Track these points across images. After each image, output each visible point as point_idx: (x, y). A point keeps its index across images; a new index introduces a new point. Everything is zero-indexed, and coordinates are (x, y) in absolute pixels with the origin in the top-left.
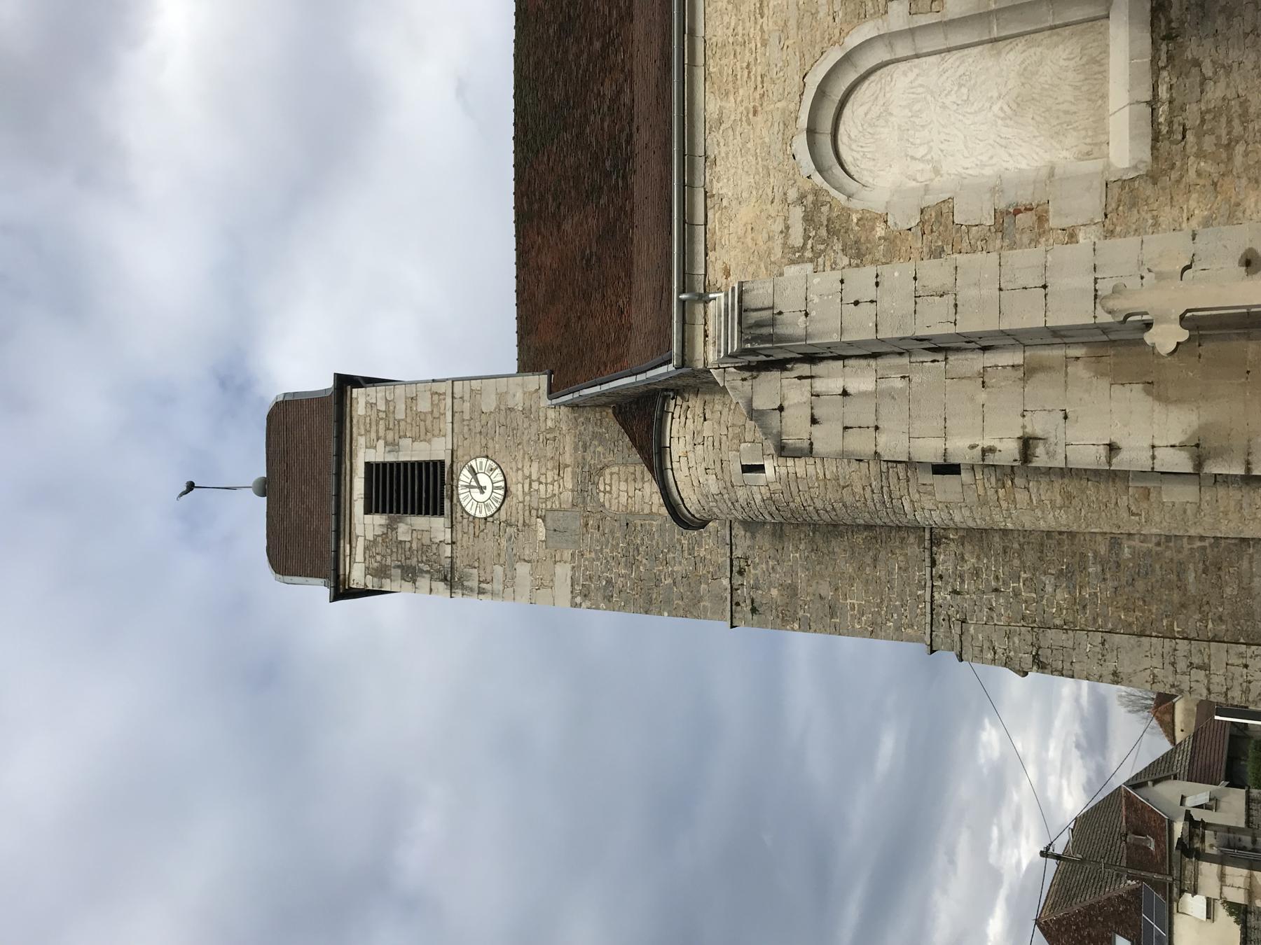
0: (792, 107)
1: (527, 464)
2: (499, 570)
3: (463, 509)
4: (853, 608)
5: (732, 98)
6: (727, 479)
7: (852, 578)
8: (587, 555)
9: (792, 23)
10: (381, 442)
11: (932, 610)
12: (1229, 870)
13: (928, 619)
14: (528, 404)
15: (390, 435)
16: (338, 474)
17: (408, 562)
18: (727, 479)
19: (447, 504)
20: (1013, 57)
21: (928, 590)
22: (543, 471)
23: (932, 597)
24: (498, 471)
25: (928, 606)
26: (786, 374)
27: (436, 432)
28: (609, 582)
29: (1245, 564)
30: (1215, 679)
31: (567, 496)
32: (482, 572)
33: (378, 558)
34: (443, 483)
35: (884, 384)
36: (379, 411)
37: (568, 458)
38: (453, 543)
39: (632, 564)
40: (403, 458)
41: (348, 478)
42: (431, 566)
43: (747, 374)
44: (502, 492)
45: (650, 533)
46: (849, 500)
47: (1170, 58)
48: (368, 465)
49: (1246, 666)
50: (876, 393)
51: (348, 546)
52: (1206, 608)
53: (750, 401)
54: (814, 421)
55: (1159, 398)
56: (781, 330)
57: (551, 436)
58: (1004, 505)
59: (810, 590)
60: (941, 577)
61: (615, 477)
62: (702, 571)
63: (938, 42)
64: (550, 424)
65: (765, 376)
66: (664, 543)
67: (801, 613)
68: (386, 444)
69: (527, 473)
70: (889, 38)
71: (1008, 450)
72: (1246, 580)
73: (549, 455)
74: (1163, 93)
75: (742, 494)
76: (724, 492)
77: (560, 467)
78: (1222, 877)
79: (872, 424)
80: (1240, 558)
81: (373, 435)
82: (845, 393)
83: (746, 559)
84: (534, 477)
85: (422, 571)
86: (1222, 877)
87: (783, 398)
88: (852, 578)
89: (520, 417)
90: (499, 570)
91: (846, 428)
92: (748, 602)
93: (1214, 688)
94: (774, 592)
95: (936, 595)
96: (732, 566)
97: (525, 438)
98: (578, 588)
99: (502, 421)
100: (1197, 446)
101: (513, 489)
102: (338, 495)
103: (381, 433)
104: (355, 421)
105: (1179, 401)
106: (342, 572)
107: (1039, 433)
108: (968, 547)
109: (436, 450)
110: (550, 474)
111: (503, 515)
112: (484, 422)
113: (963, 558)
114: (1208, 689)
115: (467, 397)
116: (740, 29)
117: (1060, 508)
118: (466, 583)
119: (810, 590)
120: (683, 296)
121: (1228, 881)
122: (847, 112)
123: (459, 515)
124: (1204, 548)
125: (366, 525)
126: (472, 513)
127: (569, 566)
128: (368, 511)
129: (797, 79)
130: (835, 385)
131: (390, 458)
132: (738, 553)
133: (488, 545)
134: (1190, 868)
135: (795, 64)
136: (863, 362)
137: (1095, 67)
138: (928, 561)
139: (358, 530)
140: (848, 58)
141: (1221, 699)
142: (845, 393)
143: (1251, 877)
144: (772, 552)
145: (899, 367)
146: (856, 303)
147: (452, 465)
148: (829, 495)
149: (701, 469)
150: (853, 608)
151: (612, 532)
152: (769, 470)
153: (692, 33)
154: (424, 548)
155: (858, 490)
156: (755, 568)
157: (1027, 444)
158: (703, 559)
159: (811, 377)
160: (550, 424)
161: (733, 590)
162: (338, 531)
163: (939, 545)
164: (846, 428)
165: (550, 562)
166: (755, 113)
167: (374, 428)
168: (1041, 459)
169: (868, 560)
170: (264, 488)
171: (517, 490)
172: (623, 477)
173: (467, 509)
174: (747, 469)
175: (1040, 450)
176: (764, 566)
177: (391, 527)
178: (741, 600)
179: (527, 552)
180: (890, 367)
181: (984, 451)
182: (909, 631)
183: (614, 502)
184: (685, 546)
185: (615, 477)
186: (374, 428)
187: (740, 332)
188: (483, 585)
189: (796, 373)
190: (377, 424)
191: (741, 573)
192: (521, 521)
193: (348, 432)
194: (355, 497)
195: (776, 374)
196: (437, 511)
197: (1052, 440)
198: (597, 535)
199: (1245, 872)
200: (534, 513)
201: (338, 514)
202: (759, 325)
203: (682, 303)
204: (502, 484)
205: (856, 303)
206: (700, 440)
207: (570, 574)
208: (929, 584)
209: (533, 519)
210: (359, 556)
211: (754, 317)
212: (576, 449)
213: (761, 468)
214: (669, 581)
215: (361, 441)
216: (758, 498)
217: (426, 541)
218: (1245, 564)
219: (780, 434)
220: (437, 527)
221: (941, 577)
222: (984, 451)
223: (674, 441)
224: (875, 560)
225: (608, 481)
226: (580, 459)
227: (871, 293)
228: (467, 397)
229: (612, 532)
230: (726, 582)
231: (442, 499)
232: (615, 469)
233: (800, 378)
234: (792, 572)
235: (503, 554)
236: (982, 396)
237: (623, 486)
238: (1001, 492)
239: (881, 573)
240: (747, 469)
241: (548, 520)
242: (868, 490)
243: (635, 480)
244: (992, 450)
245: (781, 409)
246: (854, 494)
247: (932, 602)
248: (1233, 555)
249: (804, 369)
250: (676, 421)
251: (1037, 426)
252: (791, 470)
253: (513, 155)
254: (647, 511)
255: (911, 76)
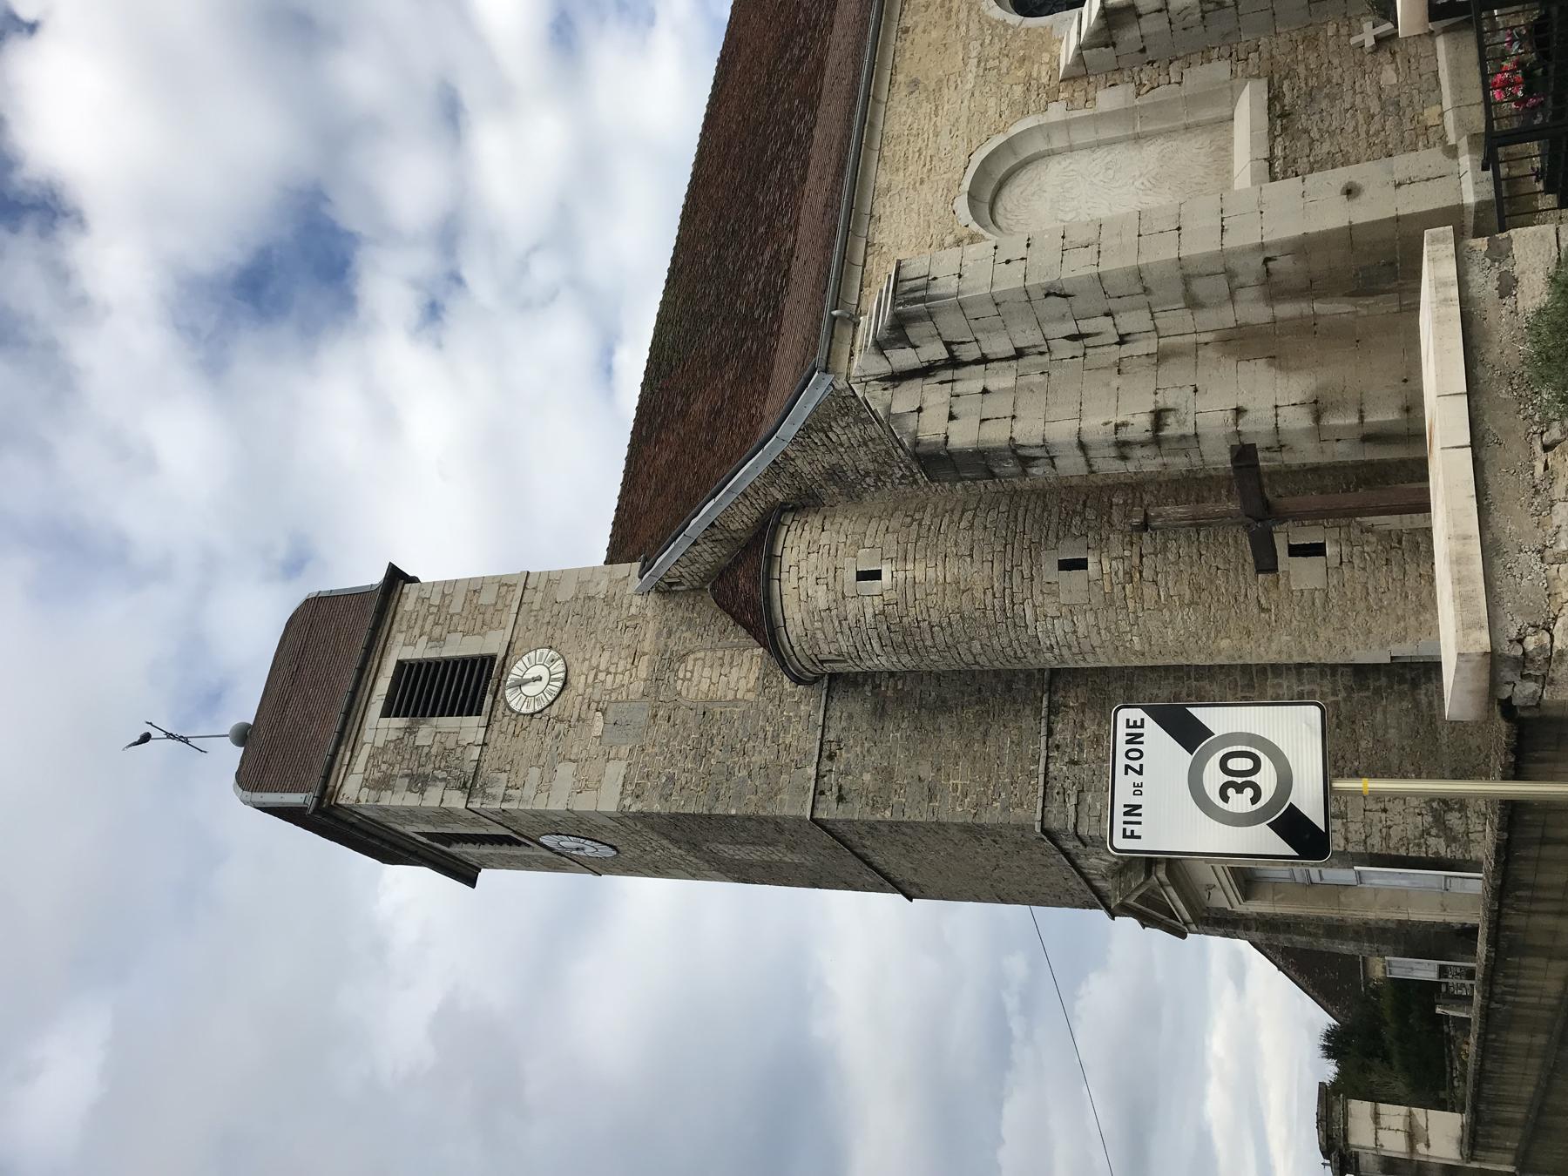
0: (957, 177)
1: (598, 651)
2: (535, 772)
3: (507, 706)
4: (955, 789)
5: (901, 173)
6: (839, 588)
7: (957, 756)
8: (650, 750)
9: (963, 119)
10: (425, 638)
11: (1046, 783)
12: (1383, 1107)
13: (1041, 793)
14: (611, 592)
15: (437, 631)
16: (362, 670)
17: (421, 770)
18: (839, 588)
19: (488, 699)
20: (1152, 151)
21: (1043, 761)
22: (615, 660)
23: (1047, 768)
24: (560, 662)
25: (1041, 778)
26: (929, 380)
27: (496, 623)
28: (671, 778)
29: (1379, 717)
30: (1352, 827)
31: (638, 687)
32: (513, 776)
33: (384, 767)
34: (489, 676)
35: (1023, 381)
36: (430, 605)
37: (647, 646)
38: (484, 744)
39: (702, 756)
40: (449, 651)
41: (386, 628)
42: (449, 773)
43: (888, 384)
44: (560, 684)
45: (730, 722)
46: (967, 608)
47: (1284, 129)
48: (400, 664)
49: (1385, 811)
50: (1015, 389)
51: (348, 754)
52: (1340, 763)
53: (890, 406)
54: (952, 417)
55: (1280, 368)
56: (932, 292)
57: (633, 624)
58: (1131, 604)
59: (908, 772)
60: (1058, 747)
61: (700, 663)
62: (784, 759)
63: (1088, 136)
64: (633, 610)
65: (905, 385)
66: (745, 730)
67: (895, 799)
68: (430, 640)
69: (594, 662)
70: (1046, 130)
71: (1140, 424)
72: (1380, 732)
73: (626, 642)
74: (1278, 152)
75: (852, 607)
76: (833, 606)
77: (635, 656)
78: (1376, 1116)
79: (1009, 413)
80: (1374, 710)
81: (417, 631)
82: (985, 391)
83: (839, 742)
84: (602, 667)
85: (436, 779)
86: (1376, 1116)
87: (923, 400)
88: (957, 756)
89: (600, 604)
90: (535, 772)
91: (983, 421)
92: (835, 789)
93: (1353, 837)
94: (867, 777)
95: (1051, 767)
96: (821, 750)
97: (601, 626)
98: (629, 788)
99: (578, 609)
100: (1316, 402)
101: (573, 680)
102: (354, 693)
103: (427, 629)
104: (398, 618)
105: (1298, 369)
106: (332, 782)
107: (1170, 404)
108: (1089, 714)
109: (492, 644)
110: (622, 663)
111: (555, 710)
112: (555, 611)
113: (1082, 726)
114: (1346, 839)
115: (541, 587)
116: (915, 126)
117: (1189, 606)
118: (488, 791)
119: (908, 772)
120: (835, 313)
121: (1384, 1122)
122: (1005, 192)
123: (499, 714)
124: (1337, 703)
125: (378, 728)
126: (517, 709)
127: (624, 764)
128: (386, 713)
129: (964, 157)
130: (977, 386)
131: (432, 654)
132: (831, 736)
133: (530, 744)
134: (1338, 1108)
135: (963, 146)
136: (1005, 364)
137: (1224, 151)
138: (1044, 731)
139: (367, 735)
140: (1009, 145)
141: (1361, 849)
142: (985, 391)
143: (1411, 1115)
144: (869, 733)
145: (1038, 365)
146: (1008, 262)
147: (505, 658)
148: (948, 604)
149: (812, 579)
150: (955, 790)
151: (684, 722)
152: (886, 576)
153: (872, 125)
154: (446, 753)
155: (979, 595)
156: (848, 752)
157: (1159, 416)
158: (788, 748)
159: (953, 381)
160: (633, 610)
161: (819, 777)
162: (341, 734)
163: (1056, 715)
164: (983, 421)
165: (602, 760)
166: (922, 182)
167: (420, 622)
168: (1172, 429)
169: (977, 736)
170: (243, 736)
171: (578, 682)
172: (708, 663)
173: (512, 705)
174: (863, 576)
175: (1171, 420)
176: (858, 749)
177: (410, 731)
178: (827, 787)
179: (575, 750)
180: (1030, 366)
181: (1117, 426)
182: (1018, 810)
183: (692, 690)
184: (769, 735)
185: (700, 663)
186: (420, 622)
187: (894, 298)
188: (510, 792)
189: (938, 379)
190: (425, 620)
191: (831, 757)
192: (575, 716)
193: (386, 628)
194: (373, 699)
195: (919, 381)
196: (474, 709)
197: (1183, 410)
198: (665, 726)
199: (1403, 1110)
200: (594, 706)
201: (347, 714)
202: (912, 290)
203: (835, 318)
204: (562, 675)
205: (1008, 262)
206: (815, 548)
207: (623, 772)
208: (1044, 754)
209: (591, 713)
210: (359, 766)
211: (908, 285)
212: (659, 635)
213: (876, 575)
214: (744, 773)
215: (400, 638)
216: (869, 611)
217: (450, 744)
218: (1379, 717)
219: (916, 432)
220: (469, 728)
221: (1058, 747)
222: (1117, 426)
223: (787, 552)
224: (986, 734)
225: (690, 668)
226: (662, 646)
227: (1023, 252)
228: (541, 587)
229: (684, 722)
230: (812, 771)
231: (484, 694)
232: (701, 654)
233: (941, 383)
234: (890, 753)
235: (544, 754)
236: (1116, 381)
237: (707, 672)
238: (1128, 587)
239: (991, 749)
240: (863, 576)
241: (610, 713)
242: (989, 593)
243: (722, 666)
244: (1125, 424)
245: (920, 410)
246: (973, 599)
247: (1046, 775)
248: (1366, 708)
249: (947, 374)
250: (792, 533)
251: (1169, 399)
252: (910, 575)
253: (619, 488)
254: (730, 696)
255: (1064, 164)
